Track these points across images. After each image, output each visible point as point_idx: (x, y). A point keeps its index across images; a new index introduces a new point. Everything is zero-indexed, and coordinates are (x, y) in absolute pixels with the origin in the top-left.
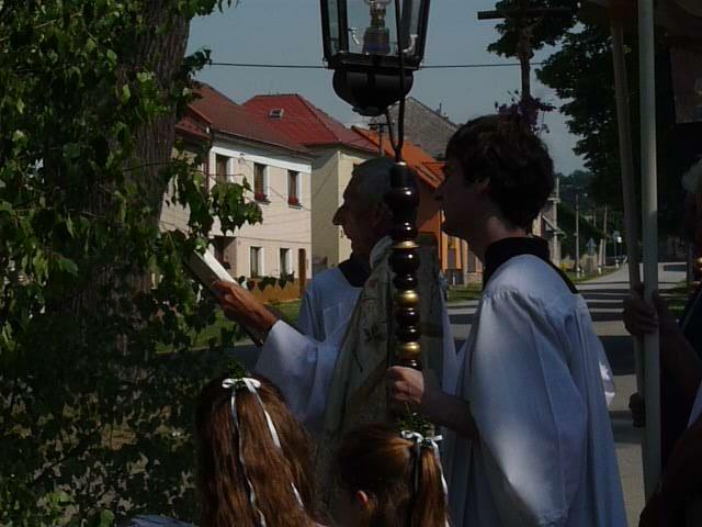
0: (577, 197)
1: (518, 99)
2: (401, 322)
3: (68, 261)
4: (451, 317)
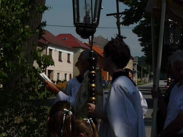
0: (142, 63)
2: (91, 92)
4: (105, 92)
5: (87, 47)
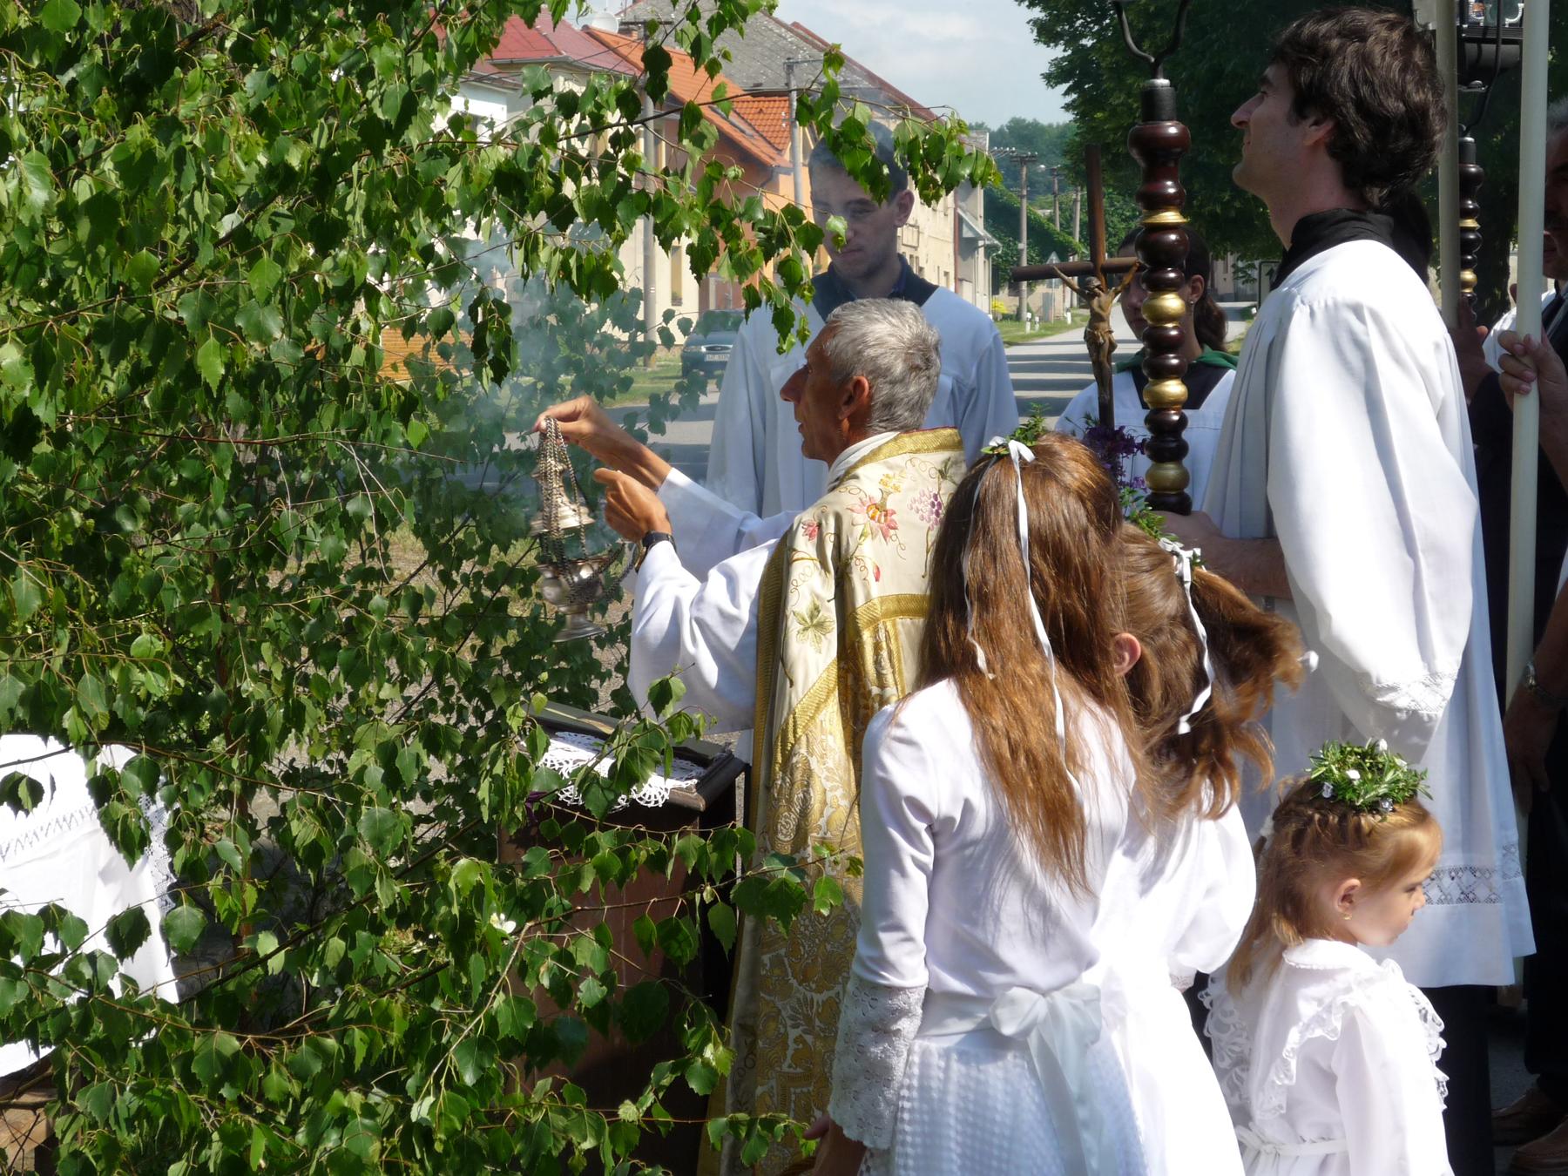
5: (607, 61)
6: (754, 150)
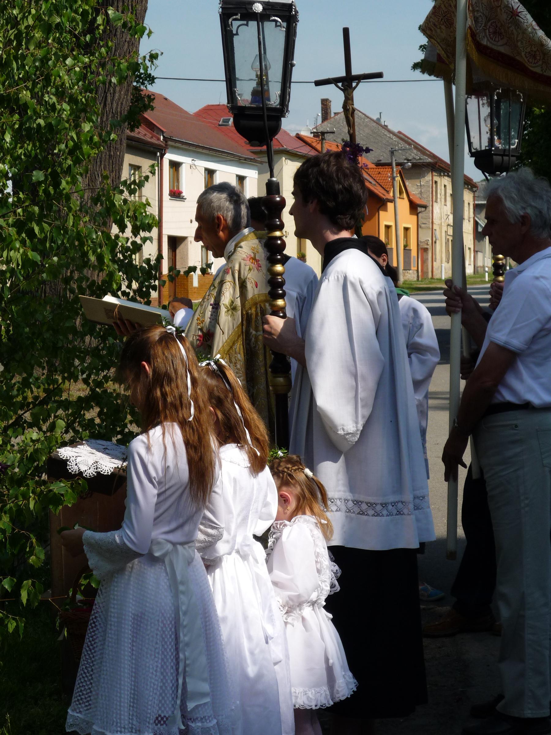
1: (346, 144)
3: (35, 253)
6: (376, 191)
